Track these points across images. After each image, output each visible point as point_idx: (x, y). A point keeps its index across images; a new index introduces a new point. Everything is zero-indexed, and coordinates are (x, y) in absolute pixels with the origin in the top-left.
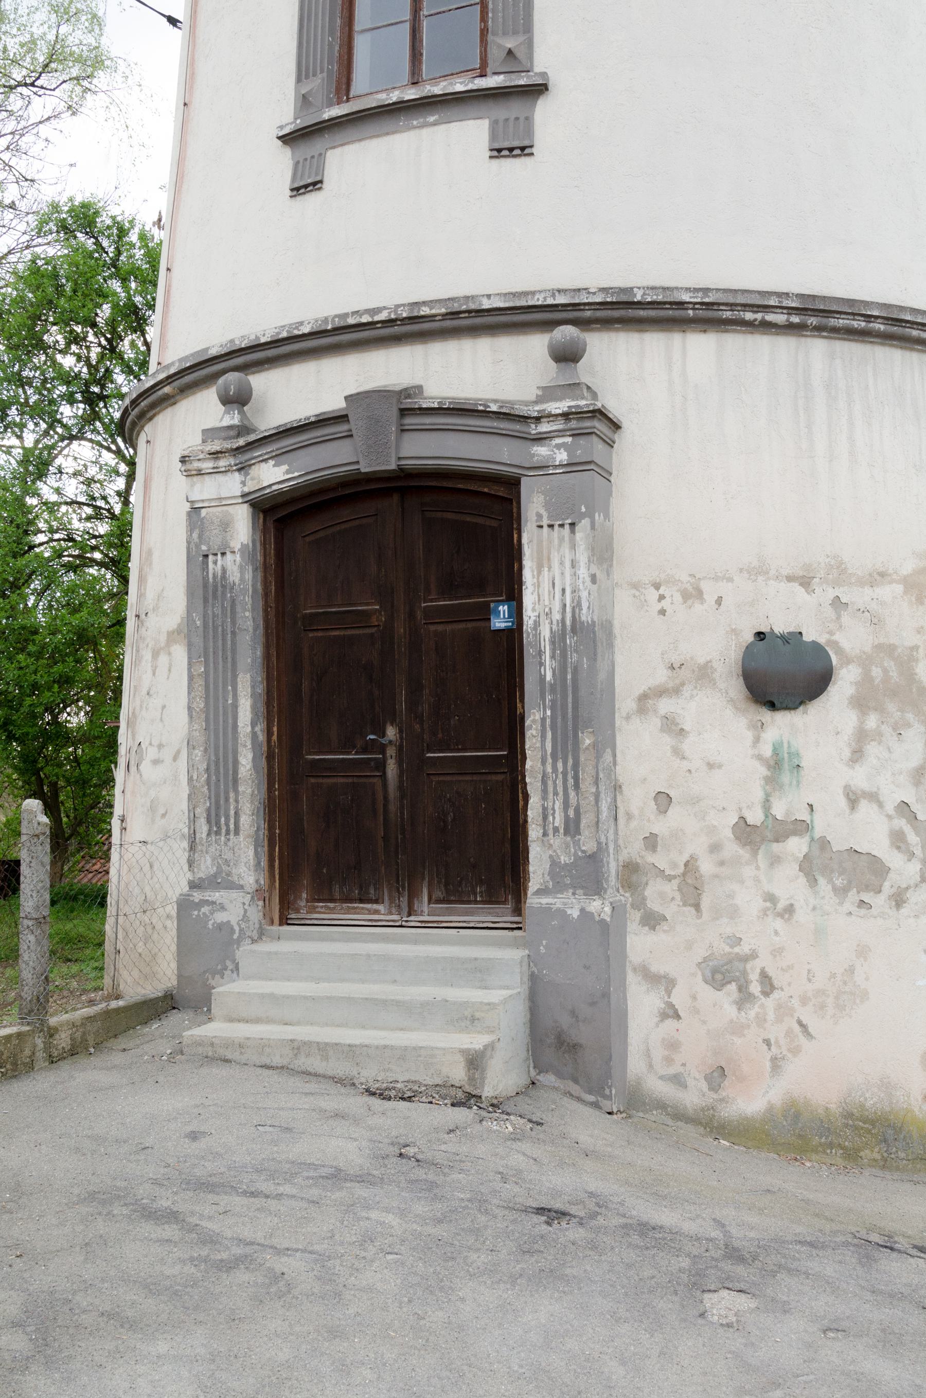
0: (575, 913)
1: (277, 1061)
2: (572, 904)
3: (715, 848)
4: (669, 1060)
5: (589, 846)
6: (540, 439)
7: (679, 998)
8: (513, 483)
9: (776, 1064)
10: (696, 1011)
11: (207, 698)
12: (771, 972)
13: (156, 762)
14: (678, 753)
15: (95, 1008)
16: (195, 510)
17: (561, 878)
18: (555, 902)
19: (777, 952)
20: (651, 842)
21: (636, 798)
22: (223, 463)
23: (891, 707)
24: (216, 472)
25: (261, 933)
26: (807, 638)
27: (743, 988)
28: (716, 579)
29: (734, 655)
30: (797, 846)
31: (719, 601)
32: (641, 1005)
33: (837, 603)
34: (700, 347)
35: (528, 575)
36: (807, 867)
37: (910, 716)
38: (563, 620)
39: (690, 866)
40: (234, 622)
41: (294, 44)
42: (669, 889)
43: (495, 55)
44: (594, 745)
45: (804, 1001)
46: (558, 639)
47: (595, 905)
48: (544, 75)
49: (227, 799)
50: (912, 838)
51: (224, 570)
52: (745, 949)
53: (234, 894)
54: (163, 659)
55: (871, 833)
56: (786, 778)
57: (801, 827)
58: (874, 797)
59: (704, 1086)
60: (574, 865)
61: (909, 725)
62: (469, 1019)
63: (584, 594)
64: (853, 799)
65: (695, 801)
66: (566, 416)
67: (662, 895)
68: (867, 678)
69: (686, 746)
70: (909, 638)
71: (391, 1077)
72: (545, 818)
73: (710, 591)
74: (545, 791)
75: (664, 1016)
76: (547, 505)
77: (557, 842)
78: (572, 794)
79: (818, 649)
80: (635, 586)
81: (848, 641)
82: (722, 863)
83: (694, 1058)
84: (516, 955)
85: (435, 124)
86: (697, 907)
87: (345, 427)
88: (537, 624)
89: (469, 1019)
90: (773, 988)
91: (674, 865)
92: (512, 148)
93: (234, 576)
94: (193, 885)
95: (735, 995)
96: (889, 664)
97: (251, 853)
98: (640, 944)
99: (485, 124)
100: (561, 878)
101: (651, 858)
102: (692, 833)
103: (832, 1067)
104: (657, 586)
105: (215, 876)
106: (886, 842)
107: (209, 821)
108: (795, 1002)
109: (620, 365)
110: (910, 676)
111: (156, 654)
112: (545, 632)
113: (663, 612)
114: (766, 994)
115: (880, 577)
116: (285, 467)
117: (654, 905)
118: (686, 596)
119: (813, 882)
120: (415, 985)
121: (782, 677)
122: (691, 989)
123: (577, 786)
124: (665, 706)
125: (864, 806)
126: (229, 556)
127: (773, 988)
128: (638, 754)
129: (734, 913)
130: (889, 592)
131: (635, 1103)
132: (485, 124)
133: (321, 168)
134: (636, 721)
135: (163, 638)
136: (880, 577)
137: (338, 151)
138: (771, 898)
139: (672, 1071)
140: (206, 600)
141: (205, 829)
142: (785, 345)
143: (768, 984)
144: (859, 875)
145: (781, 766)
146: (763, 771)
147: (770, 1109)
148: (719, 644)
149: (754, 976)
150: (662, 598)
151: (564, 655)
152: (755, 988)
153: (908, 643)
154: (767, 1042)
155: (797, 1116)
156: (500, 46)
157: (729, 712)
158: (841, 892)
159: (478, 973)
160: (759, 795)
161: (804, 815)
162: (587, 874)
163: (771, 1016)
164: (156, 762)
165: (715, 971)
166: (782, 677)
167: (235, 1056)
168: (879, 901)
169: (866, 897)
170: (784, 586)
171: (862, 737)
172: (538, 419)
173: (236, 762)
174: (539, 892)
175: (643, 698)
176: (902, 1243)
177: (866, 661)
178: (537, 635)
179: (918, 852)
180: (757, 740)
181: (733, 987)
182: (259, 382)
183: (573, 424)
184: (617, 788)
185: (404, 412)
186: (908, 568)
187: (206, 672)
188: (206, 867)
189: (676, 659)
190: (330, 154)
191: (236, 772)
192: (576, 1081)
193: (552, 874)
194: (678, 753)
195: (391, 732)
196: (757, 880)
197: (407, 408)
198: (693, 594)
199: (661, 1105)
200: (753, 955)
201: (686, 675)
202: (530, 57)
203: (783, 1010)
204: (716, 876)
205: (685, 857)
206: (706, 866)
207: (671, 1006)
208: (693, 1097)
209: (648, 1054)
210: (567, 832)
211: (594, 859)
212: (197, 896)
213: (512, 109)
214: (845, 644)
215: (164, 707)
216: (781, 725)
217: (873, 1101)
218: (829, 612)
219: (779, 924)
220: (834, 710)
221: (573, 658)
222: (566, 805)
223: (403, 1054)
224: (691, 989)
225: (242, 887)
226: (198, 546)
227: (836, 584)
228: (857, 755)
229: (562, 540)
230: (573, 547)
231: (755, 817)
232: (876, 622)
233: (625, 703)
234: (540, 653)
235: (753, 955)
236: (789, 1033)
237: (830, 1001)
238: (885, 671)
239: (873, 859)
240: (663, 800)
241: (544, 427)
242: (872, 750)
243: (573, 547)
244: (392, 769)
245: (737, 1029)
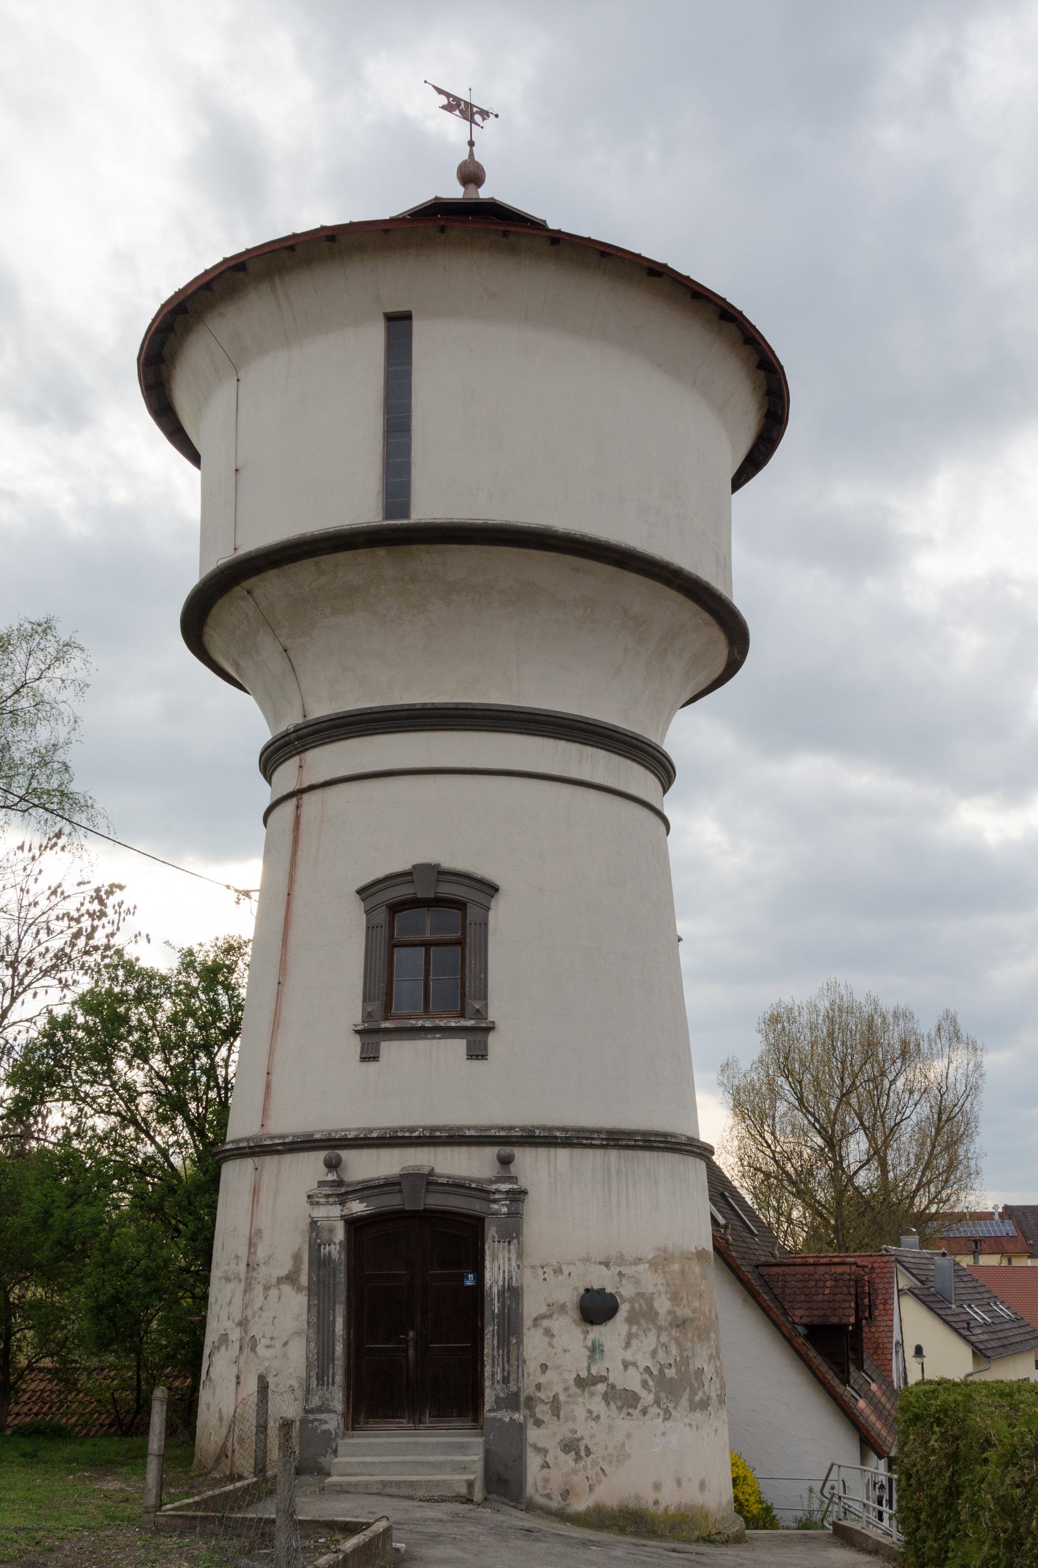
0: (507, 1420)
1: (374, 1490)
2: (505, 1416)
3: (566, 1389)
4: (545, 1487)
5: (514, 1389)
6: (495, 1201)
7: (550, 1459)
8: (480, 1220)
9: (591, 1488)
10: (557, 1464)
11: (318, 1318)
12: (590, 1446)
13: (268, 1347)
14: (550, 1345)
16: (313, 1223)
17: (500, 1404)
18: (498, 1415)
19: (592, 1437)
20: (539, 1387)
21: (532, 1367)
22: (331, 1200)
23: (643, 1322)
24: (328, 1203)
25: (344, 1434)
26: (608, 1291)
27: (577, 1454)
28: (569, 1264)
29: (576, 1299)
30: (601, 1387)
31: (570, 1274)
32: (533, 1462)
34: (563, 1155)
35: (487, 1263)
36: (606, 1397)
37: (650, 1326)
38: (504, 1285)
39: (555, 1397)
40: (334, 1280)
41: (362, 981)
42: (546, 1408)
43: (469, 1011)
44: (517, 1343)
45: (603, 1459)
46: (501, 1294)
47: (516, 1416)
48: (493, 1022)
49: (328, 1368)
50: (651, 1383)
51: (330, 1253)
52: (579, 1435)
53: (332, 1415)
54: (274, 1292)
55: (632, 1381)
56: (597, 1356)
57: (603, 1379)
58: (634, 1364)
59: (560, 1498)
60: (506, 1398)
61: (650, 1330)
62: (463, 1468)
63: (514, 1274)
64: (626, 1365)
65: (557, 1367)
66: (507, 1192)
67: (543, 1411)
68: (633, 1309)
69: (555, 1342)
70: (651, 1289)
71: (431, 1494)
72: (493, 1376)
73: (566, 1269)
74: (493, 1364)
75: (543, 1467)
76: (498, 1232)
77: (498, 1387)
78: (506, 1365)
79: (612, 1296)
80: (533, 1267)
81: (626, 1291)
82: (569, 1396)
83: (555, 1487)
84: (480, 1440)
85: (439, 1038)
86: (558, 1416)
87: (398, 1187)
88: (491, 1286)
89: (463, 1468)
90: (590, 1453)
91: (549, 1397)
92: (478, 1053)
93: (335, 1255)
94: (307, 1411)
95: (574, 1457)
96: (642, 1301)
97: (341, 1394)
98: (533, 1434)
99: (464, 1041)
100: (500, 1404)
101: (538, 1394)
102: (556, 1383)
103: (614, 1489)
104: (543, 1268)
105: (320, 1407)
106: (639, 1385)
107: (317, 1379)
108: (599, 1460)
109: (533, 1167)
110: (651, 1307)
111: (267, 1288)
112: (495, 1290)
113: (545, 1279)
114: (587, 1456)
115: (639, 1261)
116: (365, 1204)
117: (539, 1416)
118: (555, 1272)
119: (608, 1404)
120: (440, 1455)
121: (597, 1308)
122: (555, 1454)
123: (508, 1361)
124: (546, 1323)
125: (631, 1368)
126: (333, 1246)
127: (590, 1453)
128: (533, 1345)
129: (574, 1419)
130: (642, 1267)
131: (531, 1507)
132: (464, 1041)
133: (378, 1050)
134: (532, 1331)
135: (274, 1281)
136: (639, 1261)
137: (387, 1043)
138: (590, 1412)
139: (546, 1492)
140: (319, 1267)
141: (315, 1383)
142: (599, 1153)
143: (588, 1452)
144: (627, 1400)
145: (595, 1351)
146: (588, 1353)
147: (588, 1508)
148: (568, 1294)
149: (582, 1448)
150: (545, 1273)
151: (504, 1303)
152: (583, 1453)
153: (650, 1291)
154: (587, 1478)
155: (600, 1511)
156: (473, 1007)
157: (573, 1326)
158: (620, 1408)
159: (463, 1448)
160: (586, 1364)
161: (605, 1374)
162: (512, 1402)
163: (589, 1466)
164: (268, 1347)
165: (566, 1446)
166: (597, 1308)
167: (353, 1490)
168: (636, 1413)
169: (631, 1411)
171: (630, 1336)
172: (494, 1193)
173: (334, 1349)
174: (489, 1411)
175: (536, 1319)
177: (632, 1301)
178: (491, 1292)
179: (653, 1389)
180: (585, 1338)
181: (573, 1453)
182: (345, 1154)
183: (510, 1196)
184: (524, 1361)
185: (429, 1183)
186: (650, 1256)
187: (319, 1303)
188: (316, 1402)
189: (550, 1301)
190: (382, 1043)
191: (333, 1354)
192: (506, 1496)
193: (496, 1402)
194: (550, 1345)
195: (411, 1334)
196: (584, 1403)
197: (427, 1181)
198: (558, 1271)
199: (541, 1508)
200: (582, 1438)
201: (557, 1309)
202: (487, 1012)
203: (595, 1463)
204: (567, 1402)
205: (553, 1393)
206: (562, 1398)
207: (546, 1462)
208: (555, 1504)
209: (535, 1485)
210: (503, 1383)
211: (516, 1394)
212: (311, 1417)
213: (478, 1037)
214: (623, 1293)
215: (275, 1318)
216: (596, 1332)
217: (632, 1504)
218: (617, 1278)
219: (593, 1424)
220: (618, 1325)
221: (508, 1302)
222: (503, 1369)
223: (437, 1484)
224: (555, 1454)
225: (335, 1412)
226: (315, 1240)
227: (620, 1265)
228: (628, 1345)
229: (504, 1248)
230: (509, 1251)
231: (584, 1374)
232: (637, 1282)
233: (528, 1322)
234: (492, 1300)
235: (582, 1438)
236: (597, 1474)
237: (614, 1459)
238: (640, 1305)
239: (634, 1394)
240: (544, 1367)
241: (497, 1196)
242: (635, 1343)
243: (509, 1251)
244: (411, 1353)
245: (575, 1472)
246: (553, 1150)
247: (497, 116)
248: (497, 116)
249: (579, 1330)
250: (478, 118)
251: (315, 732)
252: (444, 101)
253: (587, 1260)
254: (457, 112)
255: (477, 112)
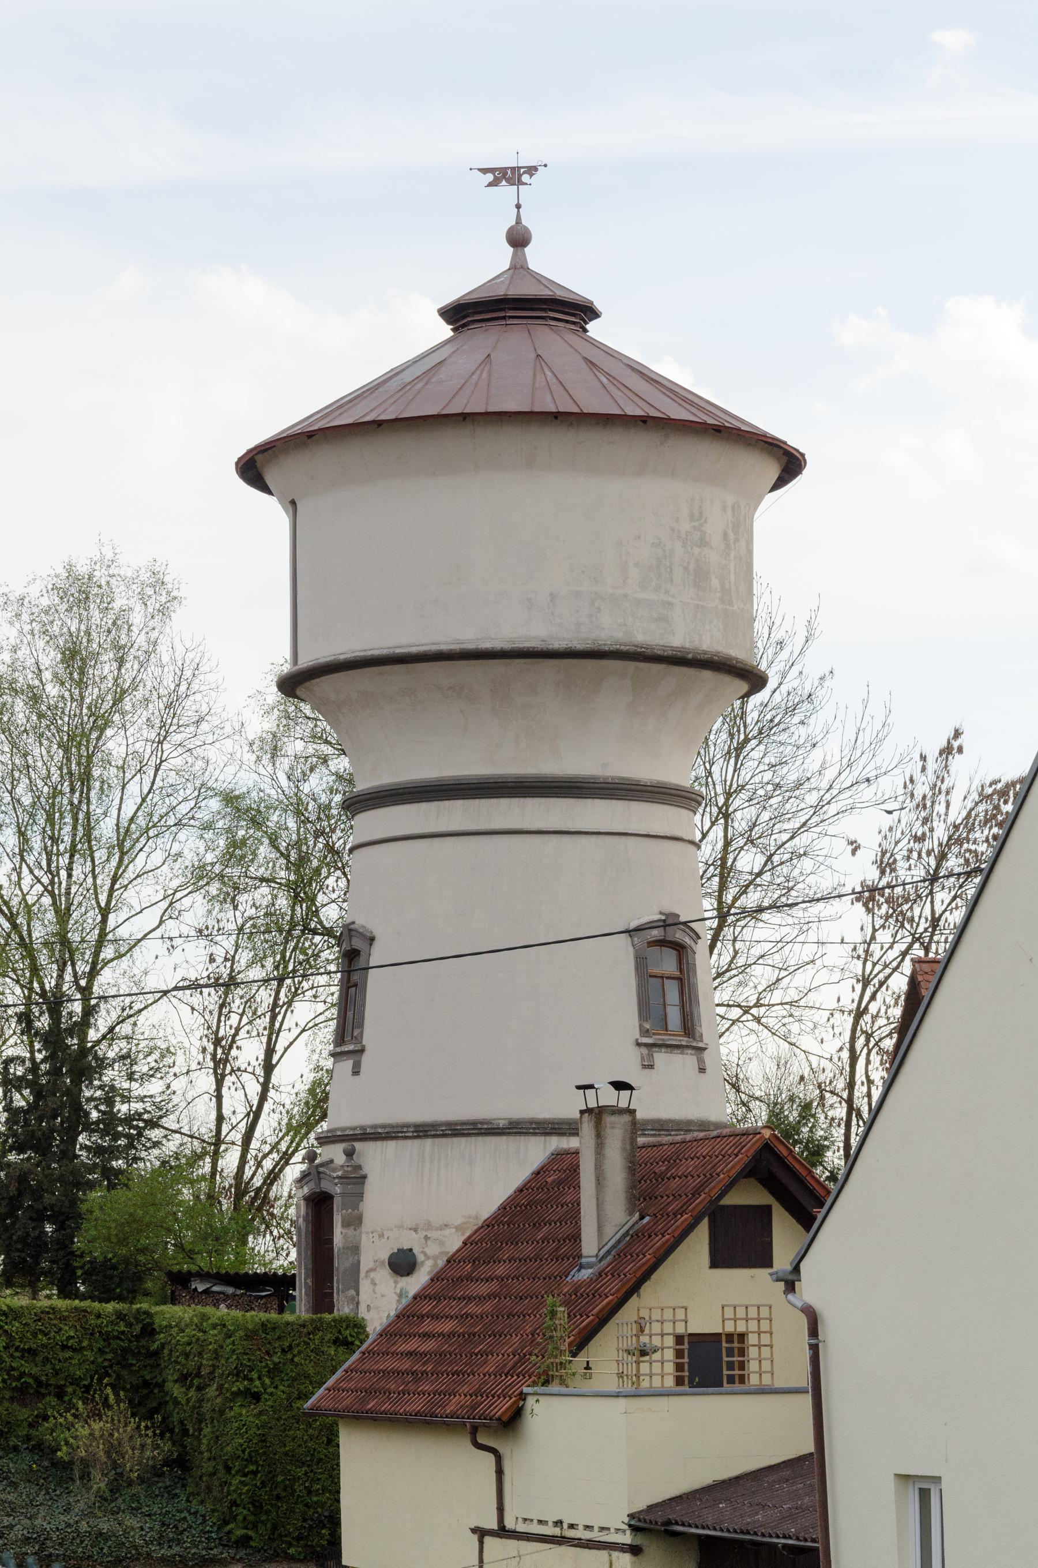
15: (68, 1302)
33: (426, 1238)
109: (374, 1157)
146: (397, 1298)
157: (274, 683)
170: (409, 1232)
176: (949, 797)
186: (458, 1222)
198: (381, 1236)
227: (427, 1230)
232: (441, 1243)
246: (548, 1138)
247: (545, 166)
248: (545, 166)
249: (392, 1281)
250: (525, 178)
251: (410, 793)
252: (490, 177)
253: (400, 1227)
254: (504, 183)
255: (525, 172)
